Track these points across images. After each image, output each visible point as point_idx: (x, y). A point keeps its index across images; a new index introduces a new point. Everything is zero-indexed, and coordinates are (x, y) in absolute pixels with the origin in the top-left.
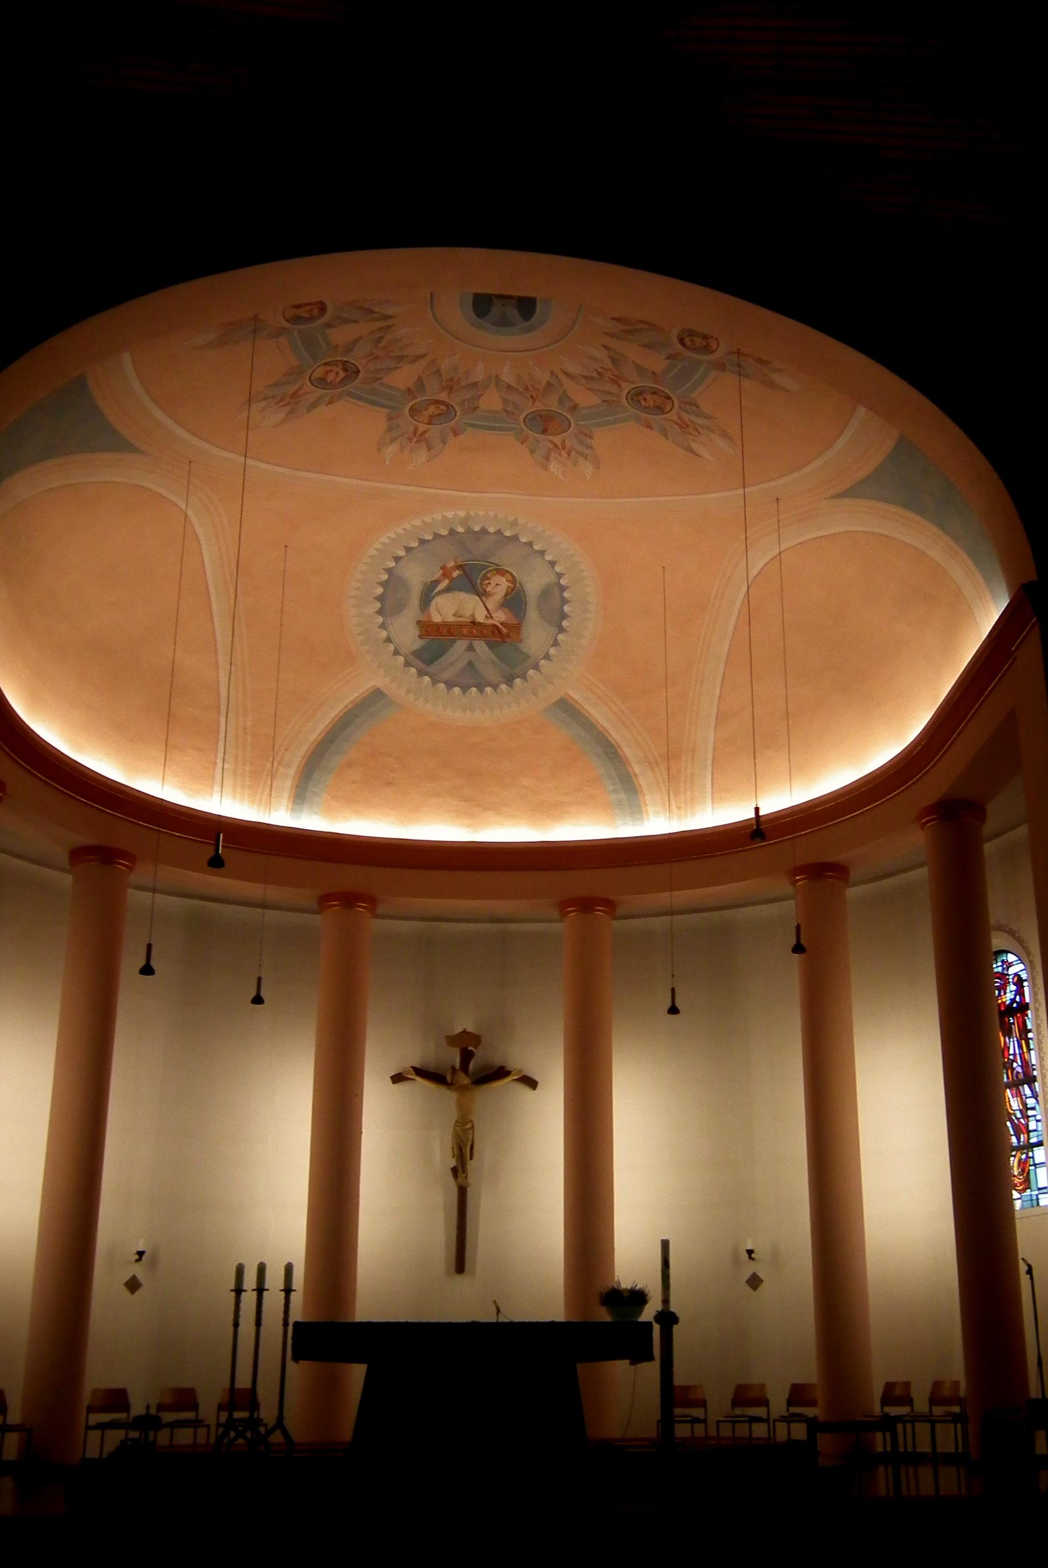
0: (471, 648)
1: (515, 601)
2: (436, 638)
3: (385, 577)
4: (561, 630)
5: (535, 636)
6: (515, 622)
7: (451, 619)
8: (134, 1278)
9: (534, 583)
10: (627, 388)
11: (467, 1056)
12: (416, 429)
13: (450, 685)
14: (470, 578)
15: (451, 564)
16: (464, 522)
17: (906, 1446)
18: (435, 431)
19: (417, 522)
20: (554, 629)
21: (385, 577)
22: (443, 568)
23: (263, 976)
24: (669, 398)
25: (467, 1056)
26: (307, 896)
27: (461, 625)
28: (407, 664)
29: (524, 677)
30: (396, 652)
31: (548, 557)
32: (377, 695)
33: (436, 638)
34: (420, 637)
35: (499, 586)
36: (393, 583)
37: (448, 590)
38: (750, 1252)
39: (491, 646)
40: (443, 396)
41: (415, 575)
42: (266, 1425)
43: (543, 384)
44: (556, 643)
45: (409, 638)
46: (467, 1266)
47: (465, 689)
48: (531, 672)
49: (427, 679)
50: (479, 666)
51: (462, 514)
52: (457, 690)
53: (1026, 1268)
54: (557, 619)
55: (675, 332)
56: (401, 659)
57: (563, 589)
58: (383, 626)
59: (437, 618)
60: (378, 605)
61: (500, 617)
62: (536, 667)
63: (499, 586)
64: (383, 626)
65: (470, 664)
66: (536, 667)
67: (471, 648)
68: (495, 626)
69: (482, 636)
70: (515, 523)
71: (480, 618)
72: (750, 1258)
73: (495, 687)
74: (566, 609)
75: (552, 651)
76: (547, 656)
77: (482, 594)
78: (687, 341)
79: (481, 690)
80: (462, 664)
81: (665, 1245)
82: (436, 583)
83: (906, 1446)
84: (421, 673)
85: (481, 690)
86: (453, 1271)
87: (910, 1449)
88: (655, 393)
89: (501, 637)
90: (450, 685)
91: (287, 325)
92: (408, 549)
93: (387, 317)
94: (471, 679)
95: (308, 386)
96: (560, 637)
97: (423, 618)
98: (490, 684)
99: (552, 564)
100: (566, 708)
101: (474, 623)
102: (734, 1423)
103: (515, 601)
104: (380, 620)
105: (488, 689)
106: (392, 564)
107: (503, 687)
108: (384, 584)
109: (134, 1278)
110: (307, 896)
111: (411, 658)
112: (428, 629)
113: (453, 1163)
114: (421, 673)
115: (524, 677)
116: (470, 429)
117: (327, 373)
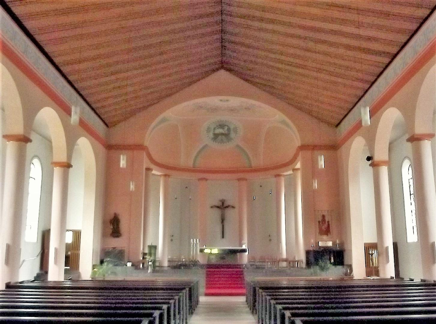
1: (229, 129)
2: (216, 136)
5: (232, 135)
9: (232, 127)
11: (223, 204)
14: (221, 126)
17: (433, 296)
23: (208, 182)
25: (223, 204)
33: (216, 136)
35: (226, 128)
45: (211, 135)
61: (226, 132)
81: (223, 237)
83: (433, 296)
86: (222, 238)
87: (435, 298)
89: (227, 135)
94: (222, 141)
100: (238, 146)
112: (215, 134)
114: (214, 141)
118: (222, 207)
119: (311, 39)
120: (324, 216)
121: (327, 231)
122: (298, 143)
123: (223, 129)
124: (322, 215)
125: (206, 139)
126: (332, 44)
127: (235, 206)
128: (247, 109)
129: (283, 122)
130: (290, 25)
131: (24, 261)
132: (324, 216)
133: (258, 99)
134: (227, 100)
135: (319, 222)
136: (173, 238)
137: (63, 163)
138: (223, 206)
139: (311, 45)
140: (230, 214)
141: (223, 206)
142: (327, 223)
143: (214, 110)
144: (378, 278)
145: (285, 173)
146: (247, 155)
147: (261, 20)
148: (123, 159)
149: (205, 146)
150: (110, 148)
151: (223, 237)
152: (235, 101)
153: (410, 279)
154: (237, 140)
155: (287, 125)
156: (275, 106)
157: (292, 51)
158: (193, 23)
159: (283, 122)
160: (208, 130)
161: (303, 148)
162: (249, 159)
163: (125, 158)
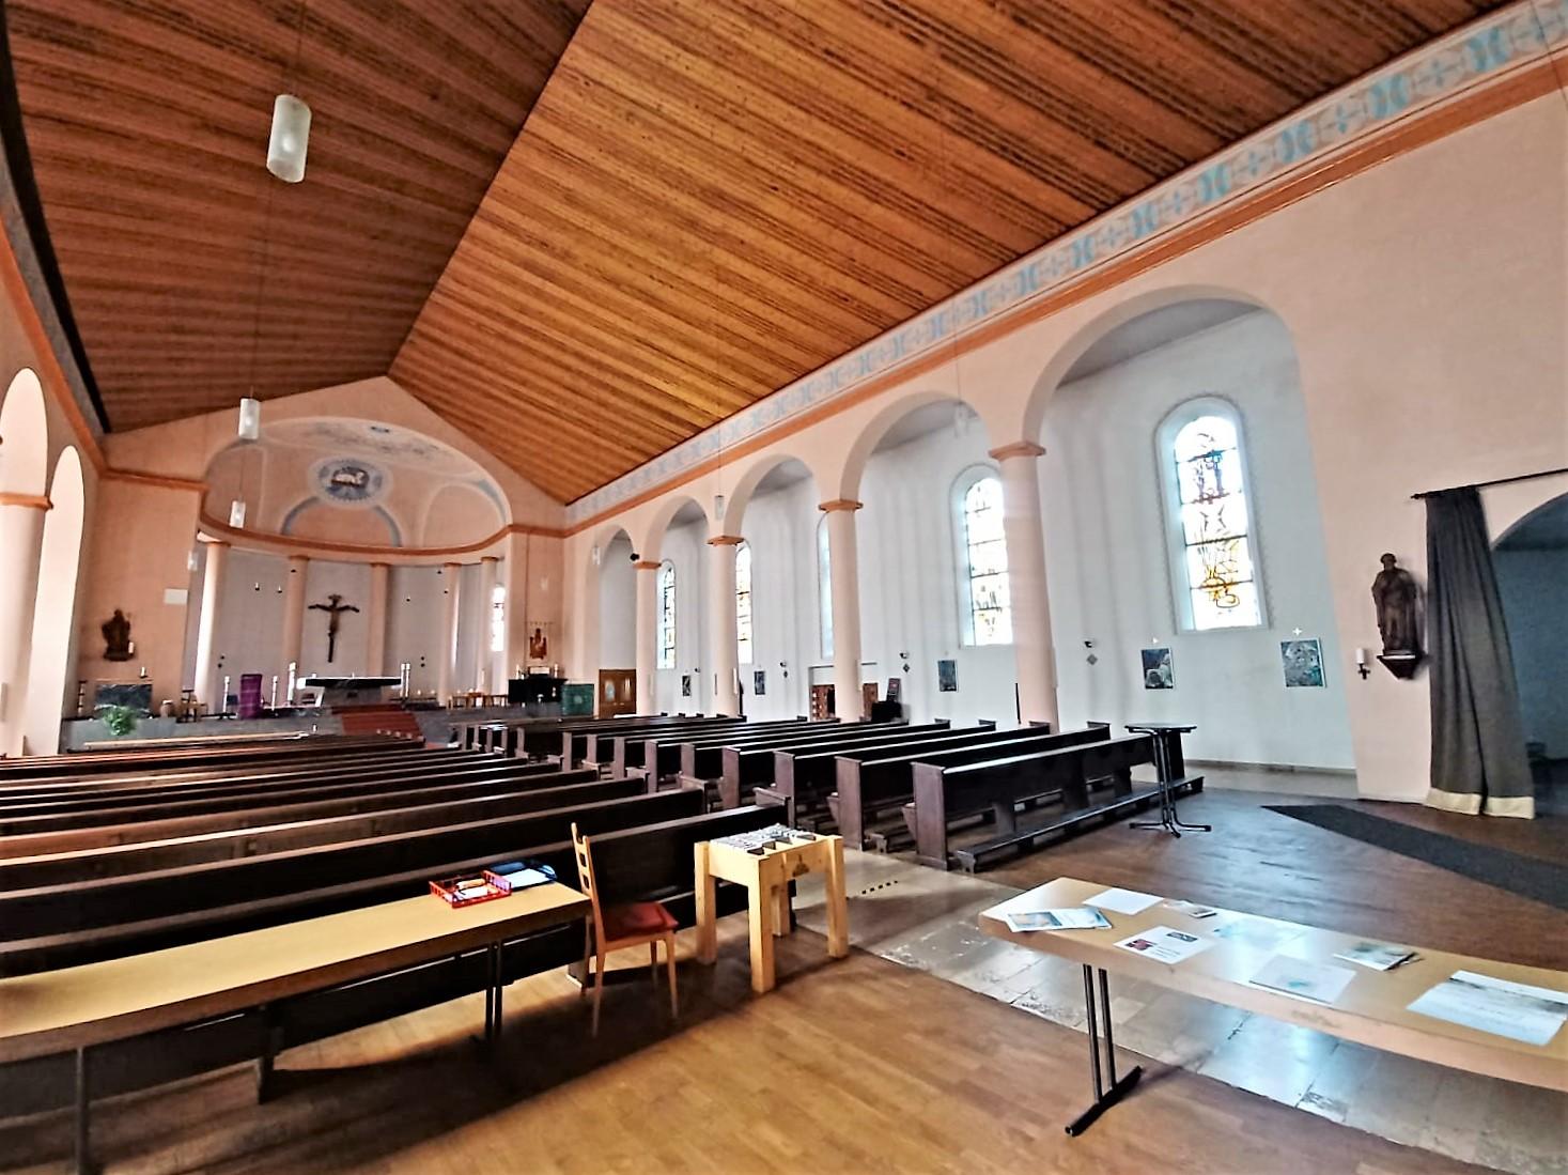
1: (366, 478)
2: (336, 486)
5: (370, 488)
9: (372, 475)
14: (352, 471)
33: (336, 486)
45: (327, 482)
61: (359, 482)
81: (330, 660)
94: (347, 496)
100: (378, 509)
112: (334, 482)
119: (587, 377)
120: (538, 631)
121: (541, 653)
122: (510, 521)
123: (354, 475)
125: (318, 488)
126: (614, 391)
128: (419, 452)
129: (483, 485)
130: (561, 347)
131: (1131, 730)
132: (538, 631)
133: (438, 436)
134: (387, 431)
136: (222, 662)
137: (33, 497)
138: (335, 608)
139: (583, 385)
140: (346, 619)
141: (335, 608)
143: (352, 440)
146: (392, 523)
147: (512, 323)
148: (239, 511)
149: (314, 500)
150: (103, 474)
151: (330, 660)
152: (400, 435)
153: (981, 722)
154: (379, 497)
155: (494, 495)
156: (475, 458)
157: (544, 384)
158: (381, 288)
159: (483, 485)
160: (323, 473)
161: (514, 528)
162: (397, 533)
163: (244, 510)
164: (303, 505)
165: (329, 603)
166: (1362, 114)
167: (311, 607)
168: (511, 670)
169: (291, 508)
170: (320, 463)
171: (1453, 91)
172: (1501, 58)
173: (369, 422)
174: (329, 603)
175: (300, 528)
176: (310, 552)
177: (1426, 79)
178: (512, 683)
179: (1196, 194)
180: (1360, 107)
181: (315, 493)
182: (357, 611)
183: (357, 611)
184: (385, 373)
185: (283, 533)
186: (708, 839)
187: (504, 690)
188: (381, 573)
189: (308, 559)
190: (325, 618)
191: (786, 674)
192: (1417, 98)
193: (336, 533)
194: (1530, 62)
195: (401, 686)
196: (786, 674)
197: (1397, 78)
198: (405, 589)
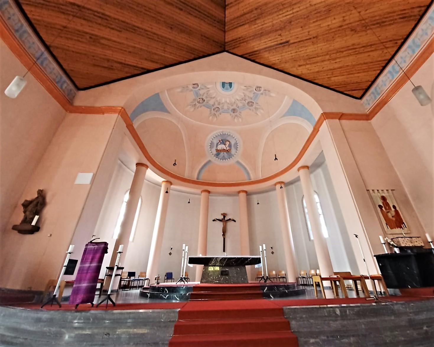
0: (224, 153)
1: (230, 146)
3: (211, 142)
4: (237, 150)
5: (233, 151)
6: (230, 149)
7: (221, 149)
8: (171, 253)
9: (233, 143)
10: (247, 101)
11: (224, 217)
12: (214, 113)
13: (221, 159)
14: (223, 142)
15: (220, 140)
16: (222, 132)
18: (217, 114)
19: (215, 132)
20: (235, 150)
21: (211, 142)
22: (219, 141)
24: (253, 103)
25: (224, 217)
26: (199, 191)
27: (222, 150)
28: (214, 156)
29: (232, 158)
30: (213, 154)
31: (235, 138)
32: (210, 161)
34: (216, 152)
35: (228, 143)
36: (212, 143)
37: (220, 144)
38: (272, 248)
39: (226, 153)
40: (218, 106)
41: (215, 142)
42: (295, 283)
43: (233, 102)
44: (236, 152)
45: (215, 152)
46: (225, 251)
47: (223, 160)
48: (233, 157)
49: (217, 158)
50: (225, 156)
51: (222, 130)
52: (222, 160)
53: (355, 236)
54: (236, 149)
55: (254, 88)
56: (213, 155)
57: (237, 143)
58: (211, 150)
59: (218, 149)
60: (210, 147)
61: (228, 148)
62: (233, 156)
63: (228, 143)
64: (211, 150)
65: (224, 156)
66: (233, 156)
67: (224, 153)
68: (227, 150)
69: (225, 151)
70: (230, 132)
71: (225, 149)
72: (272, 249)
73: (227, 159)
74: (238, 147)
75: (236, 153)
76: (235, 154)
77: (225, 145)
78: (257, 90)
79: (225, 160)
80: (223, 156)
81: (224, 251)
82: (219, 143)
84: (216, 157)
85: (225, 160)
88: (251, 102)
90: (221, 159)
91: (193, 89)
92: (214, 137)
93: (208, 88)
94: (224, 158)
95: (197, 103)
96: (237, 151)
97: (216, 149)
98: (227, 159)
99: (236, 139)
100: (238, 162)
101: (224, 150)
102: (279, 278)
103: (230, 146)
104: (210, 149)
105: (226, 160)
106: (212, 140)
107: (229, 159)
108: (211, 143)
109: (171, 253)
110: (199, 191)
111: (215, 155)
112: (217, 150)
113: (222, 234)
114: (216, 157)
115: (232, 158)
116: (223, 113)
117: (200, 100)
118: (223, 220)
124: (380, 197)
127: (261, 86)
135: (380, 206)
140: (230, 224)
141: (224, 220)
142: (393, 209)
144: (338, 276)
145: (180, 309)
146: (245, 169)
151: (224, 251)
154: (238, 156)
162: (248, 173)
164: (205, 165)
165: (221, 217)
166: (409, 55)
167: (214, 220)
168: (373, 244)
169: (200, 167)
170: (209, 138)
171: (373, 105)
172: (418, 46)
173: (219, 78)
174: (221, 217)
175: (204, 177)
176: (210, 188)
177: (422, 36)
178: (380, 258)
179: (372, 98)
180: (407, 54)
181: (210, 159)
182: (235, 221)
183: (235, 221)
184: (222, 47)
185: (198, 179)
186: (358, 288)
187: (375, 270)
188: (243, 195)
189: (209, 192)
190: (220, 225)
191: (170, 254)
192: (422, 42)
193: (221, 178)
194: (400, 74)
195: (261, 265)
196: (170, 254)
197: (414, 41)
198: (256, 209)
